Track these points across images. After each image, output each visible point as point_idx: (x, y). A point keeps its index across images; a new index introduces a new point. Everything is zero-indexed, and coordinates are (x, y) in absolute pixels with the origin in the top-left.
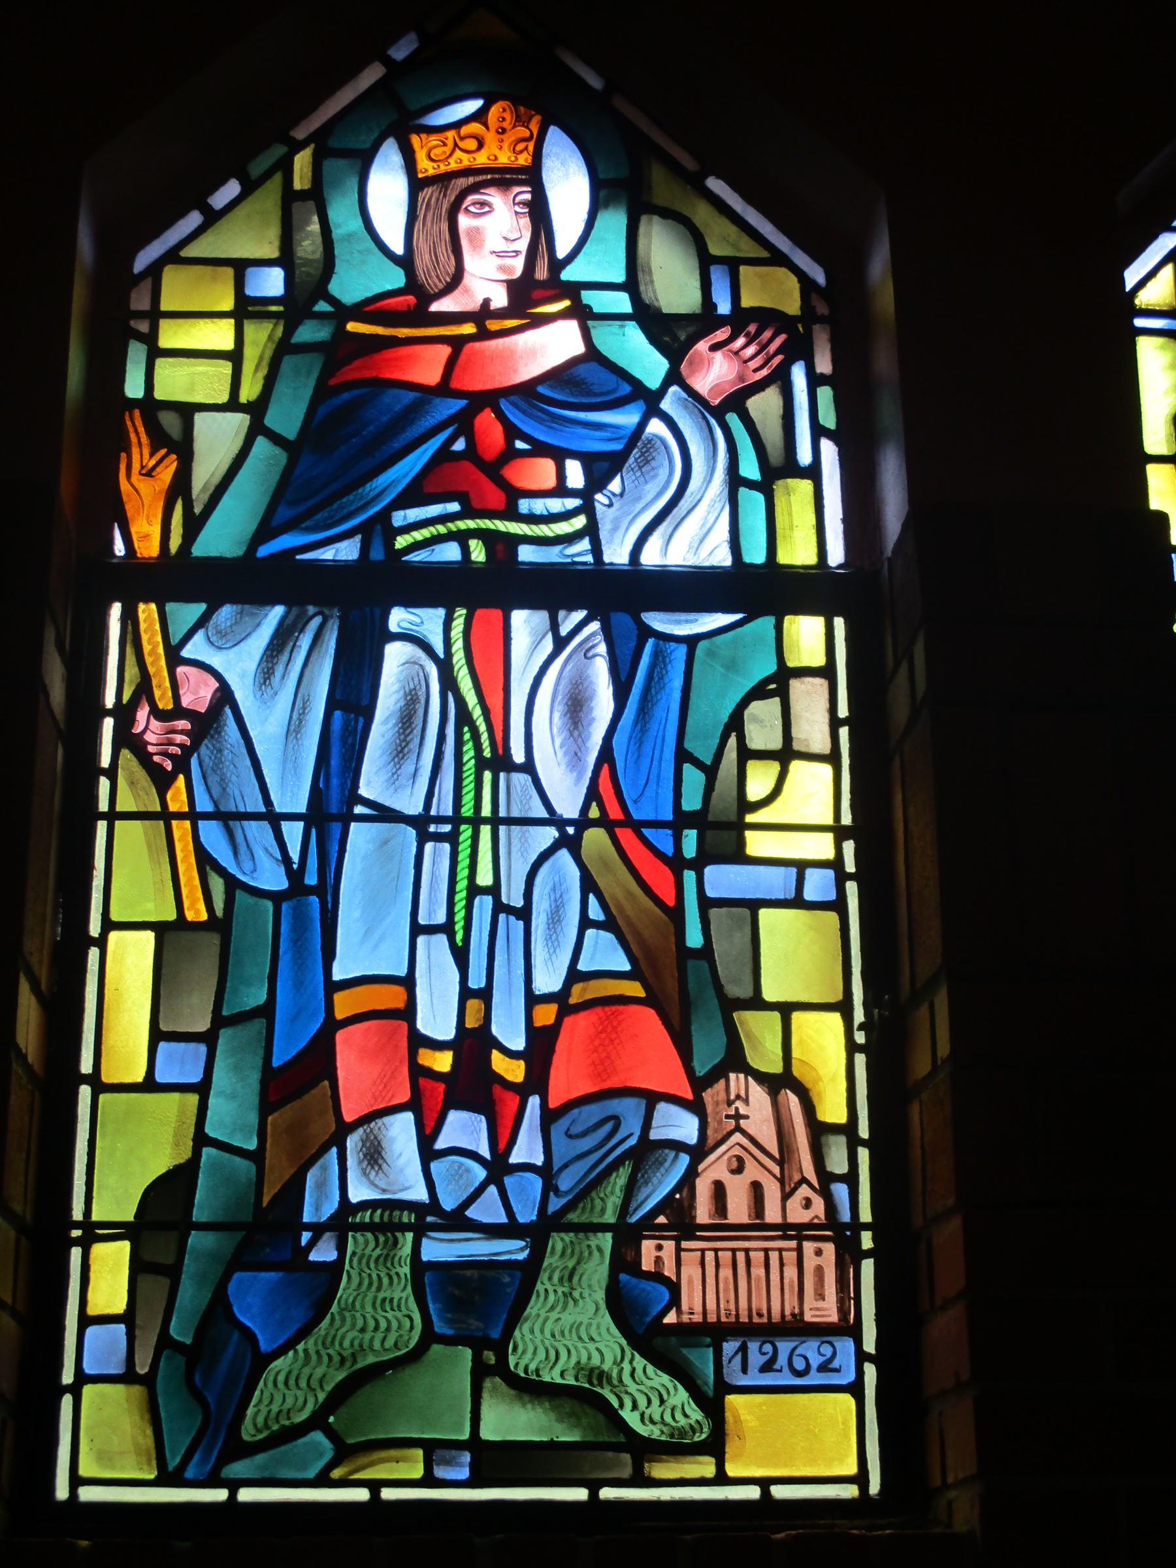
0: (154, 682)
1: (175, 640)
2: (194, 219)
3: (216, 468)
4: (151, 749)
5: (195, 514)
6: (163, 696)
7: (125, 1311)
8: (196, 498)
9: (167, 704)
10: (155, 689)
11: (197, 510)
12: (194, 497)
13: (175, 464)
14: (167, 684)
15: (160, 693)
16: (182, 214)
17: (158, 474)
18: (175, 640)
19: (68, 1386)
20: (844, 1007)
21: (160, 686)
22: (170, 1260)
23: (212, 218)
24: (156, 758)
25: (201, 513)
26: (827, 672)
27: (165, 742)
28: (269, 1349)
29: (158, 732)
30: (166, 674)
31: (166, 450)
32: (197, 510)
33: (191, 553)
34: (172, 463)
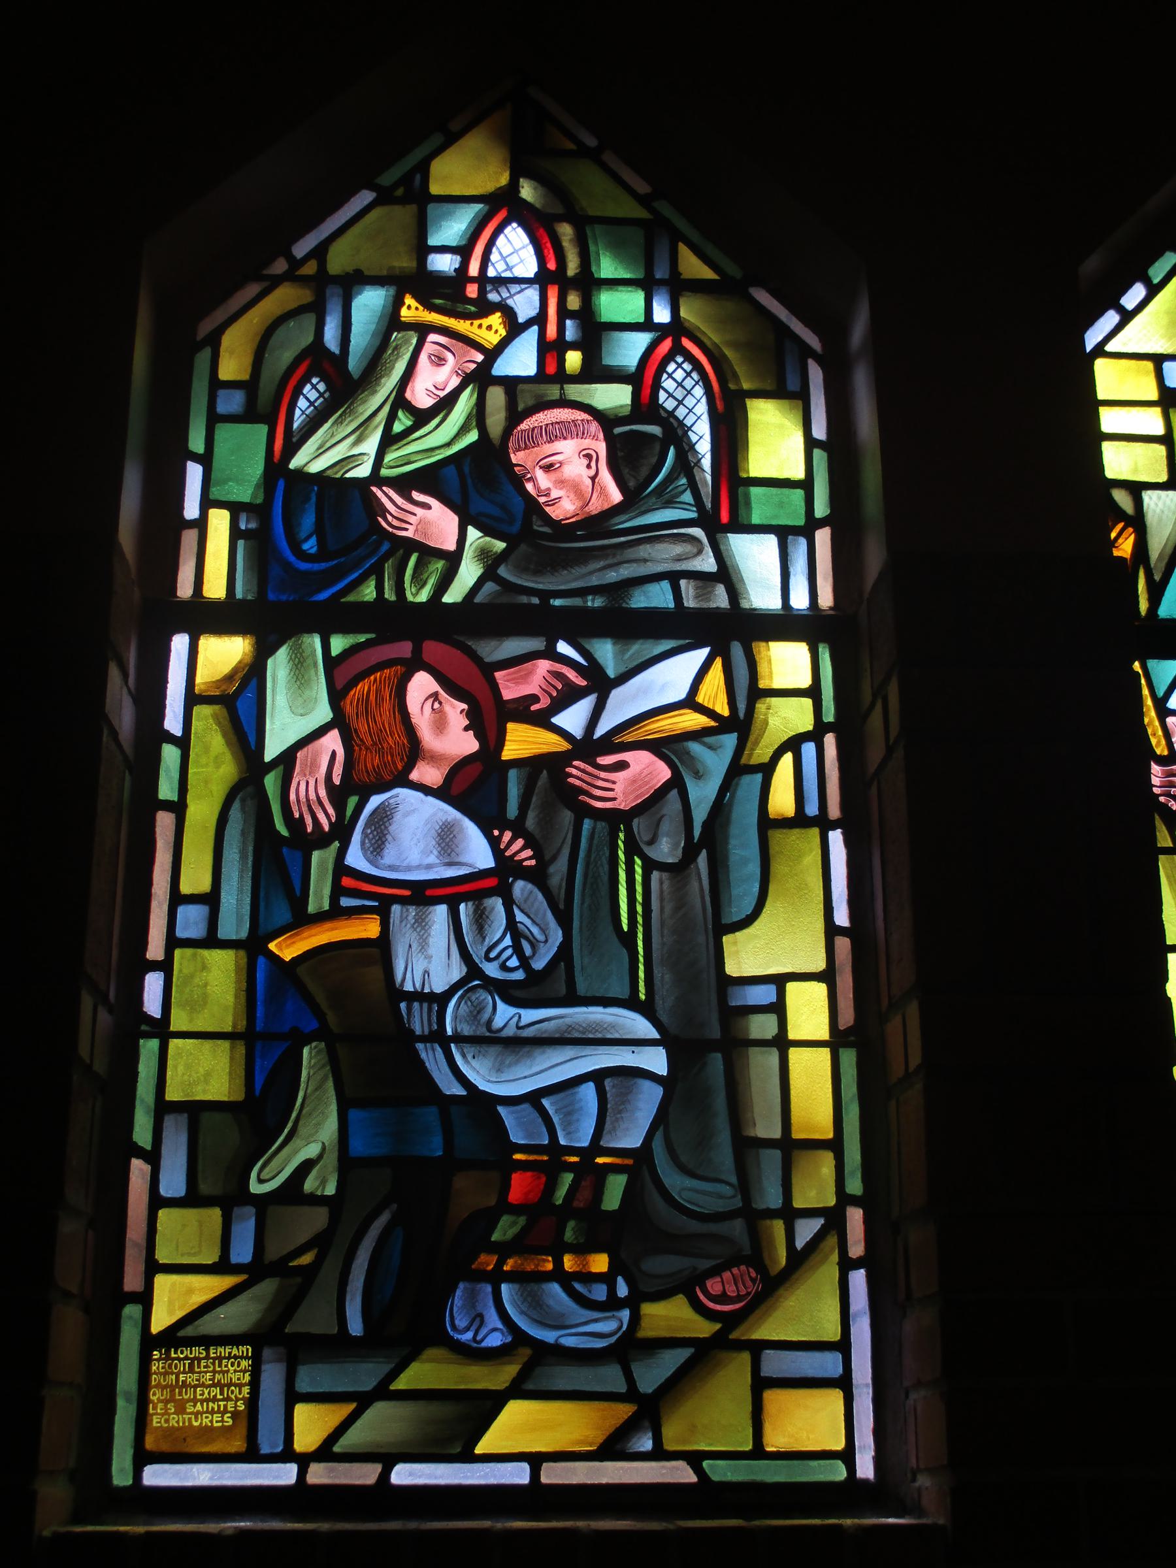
0: (1150, 731)
1: (1160, 693)
2: (1111, 319)
3: (1170, 535)
4: (1156, 790)
5: (1155, 581)
6: (1158, 743)
7: (146, 1013)
8: (1154, 566)
9: (1163, 750)
10: (1150, 737)
11: (1157, 577)
12: (1152, 566)
13: (1132, 537)
14: (1160, 733)
15: (1156, 740)
16: (1100, 314)
17: (1121, 545)
18: (1160, 693)
19: (857, 1268)
20: (827, 976)
21: (1155, 735)
22: (265, 1450)
23: (1127, 317)
24: (1162, 799)
25: (1161, 580)
26: (835, 1145)
27: (1167, 784)
28: (412, 333)
29: (1160, 775)
30: (1157, 723)
31: (1123, 524)
32: (1157, 577)
33: (1158, 616)
34: (1130, 535)
